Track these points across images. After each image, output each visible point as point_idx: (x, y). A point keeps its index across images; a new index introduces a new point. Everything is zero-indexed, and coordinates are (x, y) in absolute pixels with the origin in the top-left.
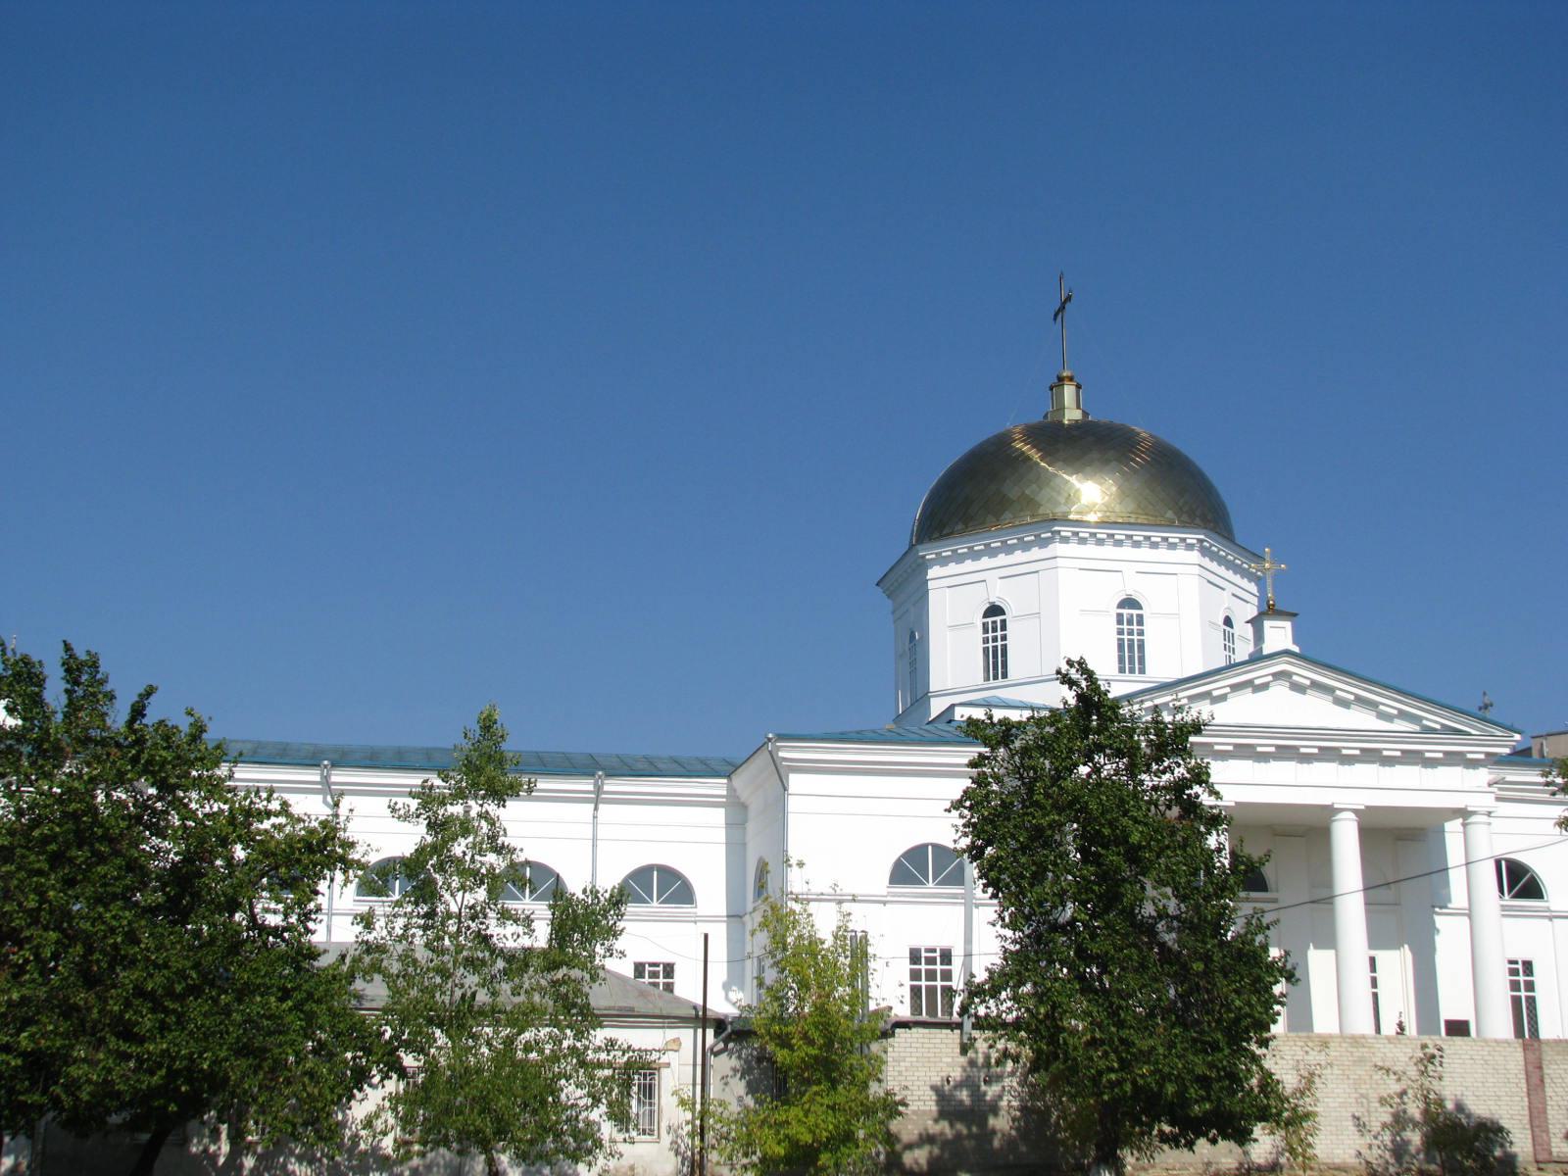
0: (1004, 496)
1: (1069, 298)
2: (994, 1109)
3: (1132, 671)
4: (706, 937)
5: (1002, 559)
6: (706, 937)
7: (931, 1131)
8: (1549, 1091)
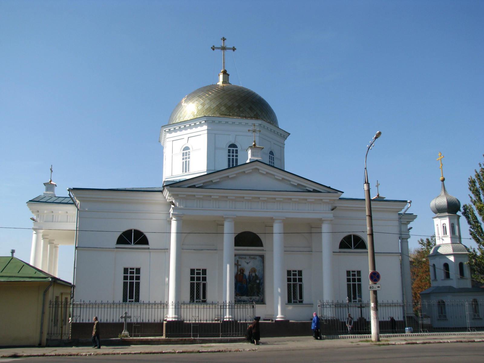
4: (184, 138)
6: (184, 138)
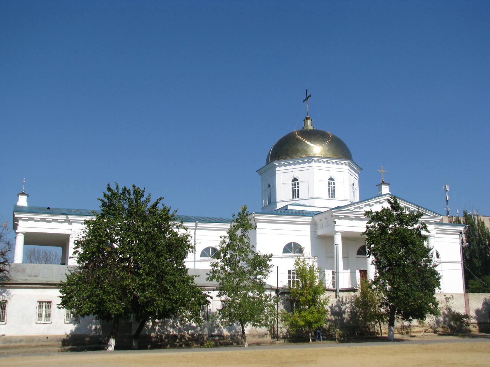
0: (298, 149)
1: (310, 96)
2: (344, 312)
3: (332, 197)
4: (278, 267)
5: (297, 166)
6: (278, 267)
7: (329, 318)
8: (470, 306)
